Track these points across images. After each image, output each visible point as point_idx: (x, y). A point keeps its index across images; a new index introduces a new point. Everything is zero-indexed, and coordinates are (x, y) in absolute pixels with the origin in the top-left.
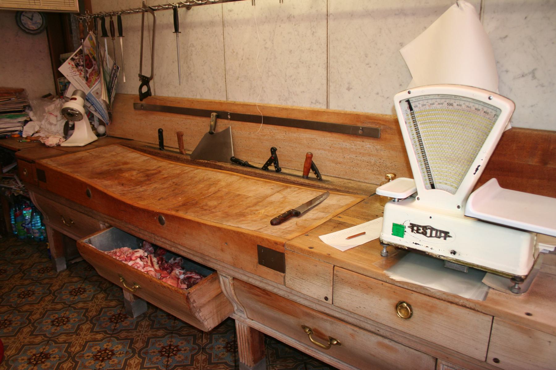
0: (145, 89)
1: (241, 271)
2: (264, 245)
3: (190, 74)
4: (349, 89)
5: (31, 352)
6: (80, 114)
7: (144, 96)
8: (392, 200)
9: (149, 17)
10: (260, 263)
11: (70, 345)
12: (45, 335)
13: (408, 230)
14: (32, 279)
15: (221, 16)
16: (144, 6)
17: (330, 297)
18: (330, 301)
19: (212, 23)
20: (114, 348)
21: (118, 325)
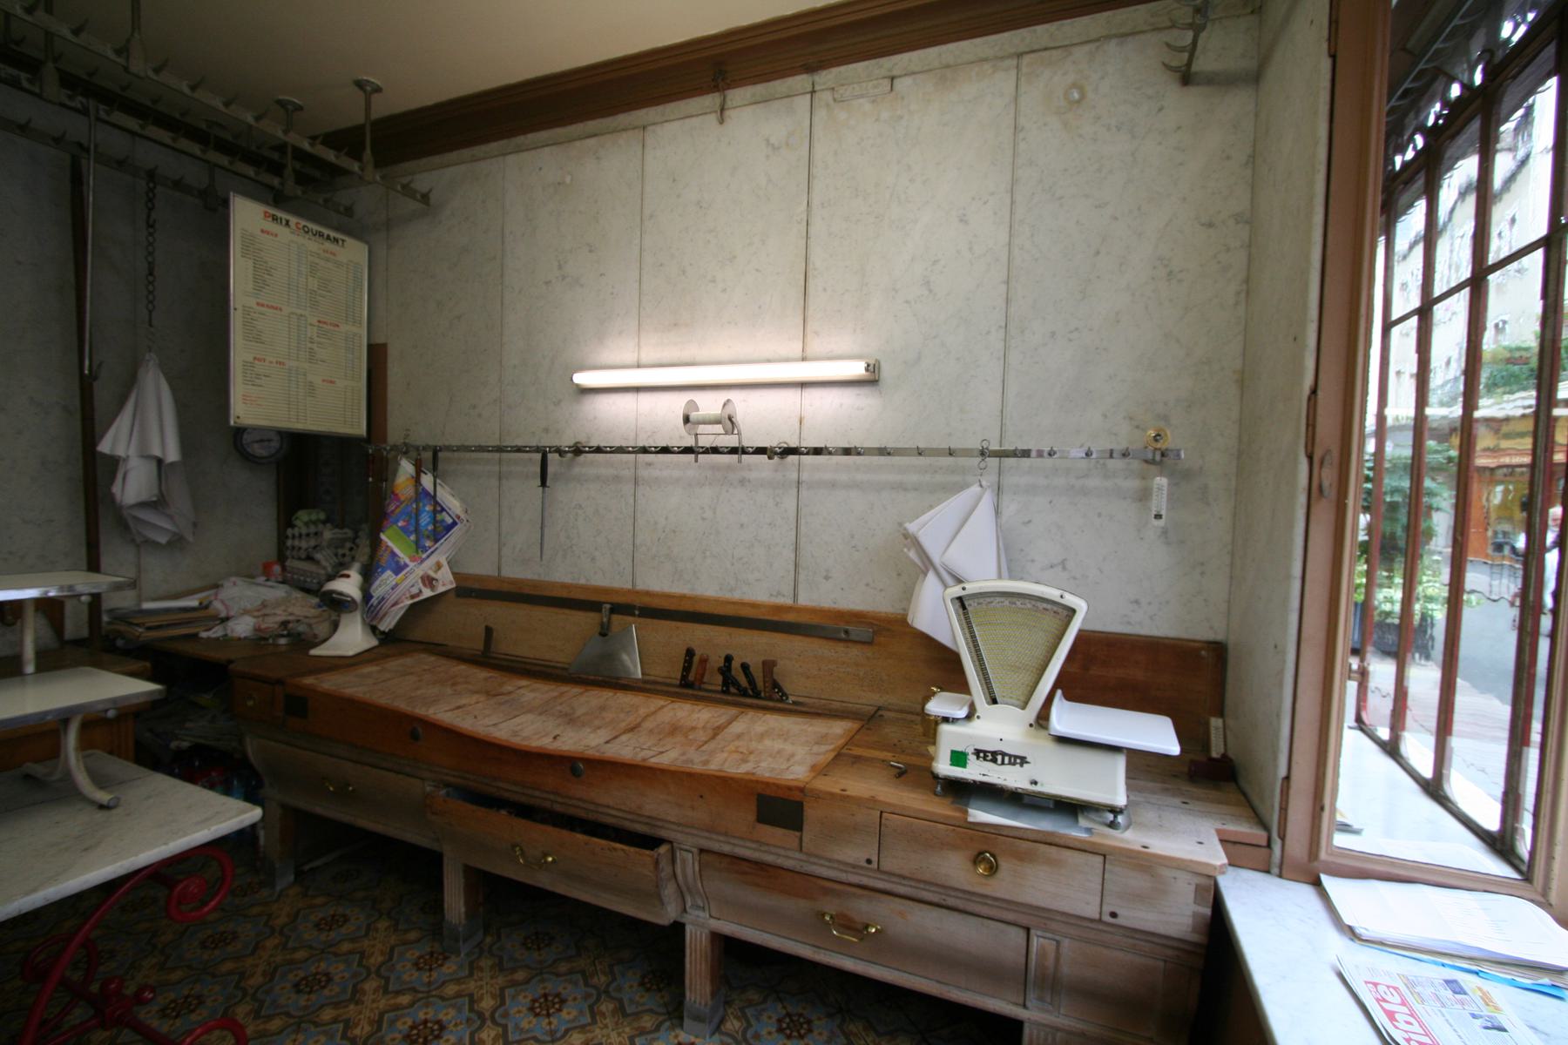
2: (768, 792)
4: (827, 578)
6: (353, 601)
8: (946, 720)
11: (348, 1025)
13: (972, 758)
17: (874, 859)
18: (875, 865)
19: (617, 479)
20: (441, 1016)
21: (435, 974)
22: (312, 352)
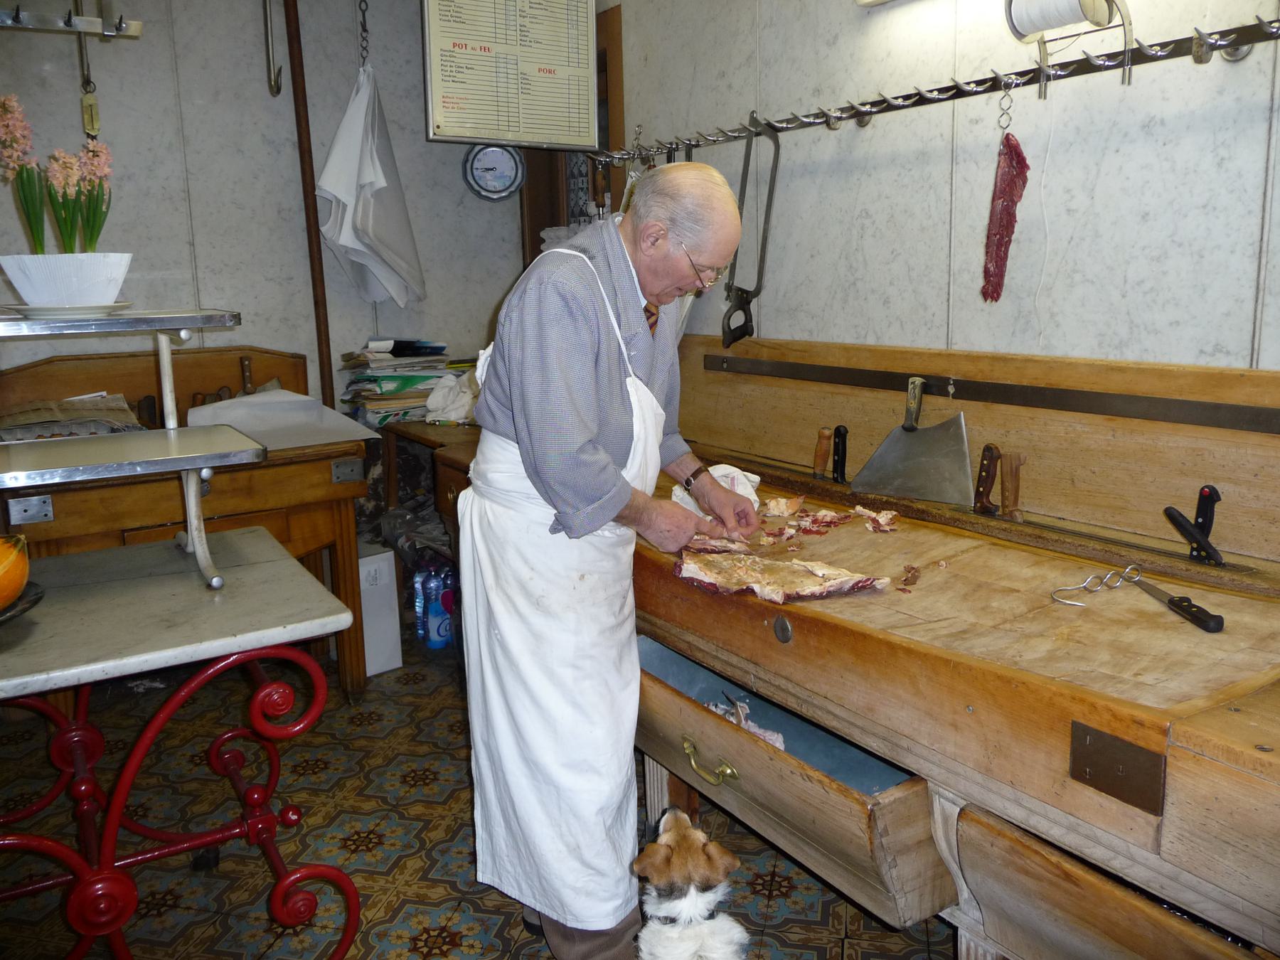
0: (738, 320)
1: (1008, 791)
2: (1093, 723)
3: (854, 284)
5: (420, 923)
7: (735, 335)
9: (763, 145)
10: (1078, 773)
12: (453, 885)
14: (435, 745)
15: (948, 136)
16: (754, 121)
22: (523, 31)
